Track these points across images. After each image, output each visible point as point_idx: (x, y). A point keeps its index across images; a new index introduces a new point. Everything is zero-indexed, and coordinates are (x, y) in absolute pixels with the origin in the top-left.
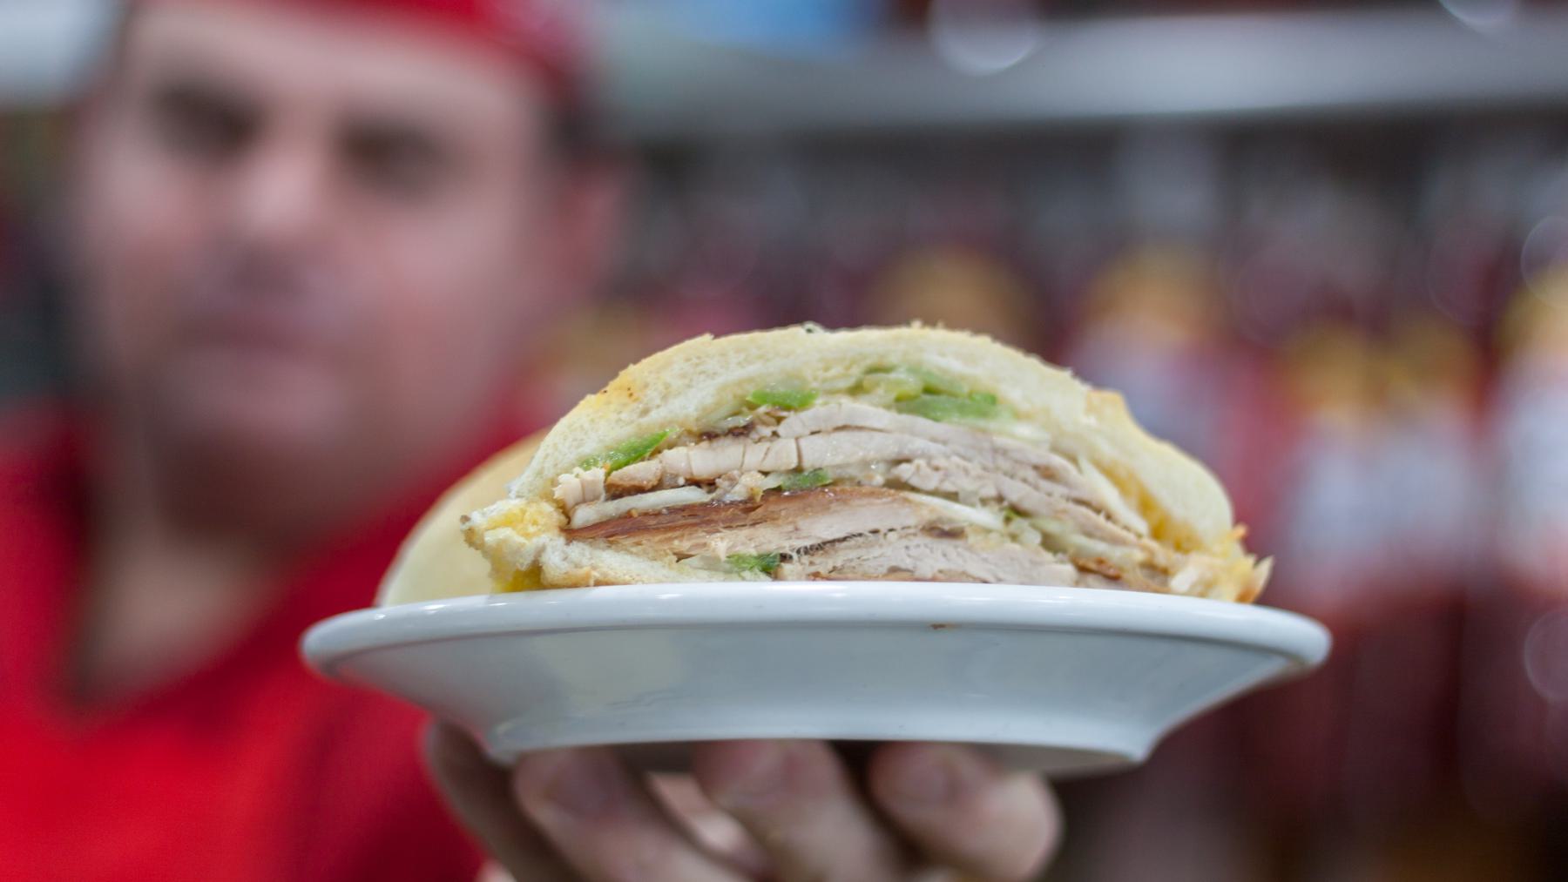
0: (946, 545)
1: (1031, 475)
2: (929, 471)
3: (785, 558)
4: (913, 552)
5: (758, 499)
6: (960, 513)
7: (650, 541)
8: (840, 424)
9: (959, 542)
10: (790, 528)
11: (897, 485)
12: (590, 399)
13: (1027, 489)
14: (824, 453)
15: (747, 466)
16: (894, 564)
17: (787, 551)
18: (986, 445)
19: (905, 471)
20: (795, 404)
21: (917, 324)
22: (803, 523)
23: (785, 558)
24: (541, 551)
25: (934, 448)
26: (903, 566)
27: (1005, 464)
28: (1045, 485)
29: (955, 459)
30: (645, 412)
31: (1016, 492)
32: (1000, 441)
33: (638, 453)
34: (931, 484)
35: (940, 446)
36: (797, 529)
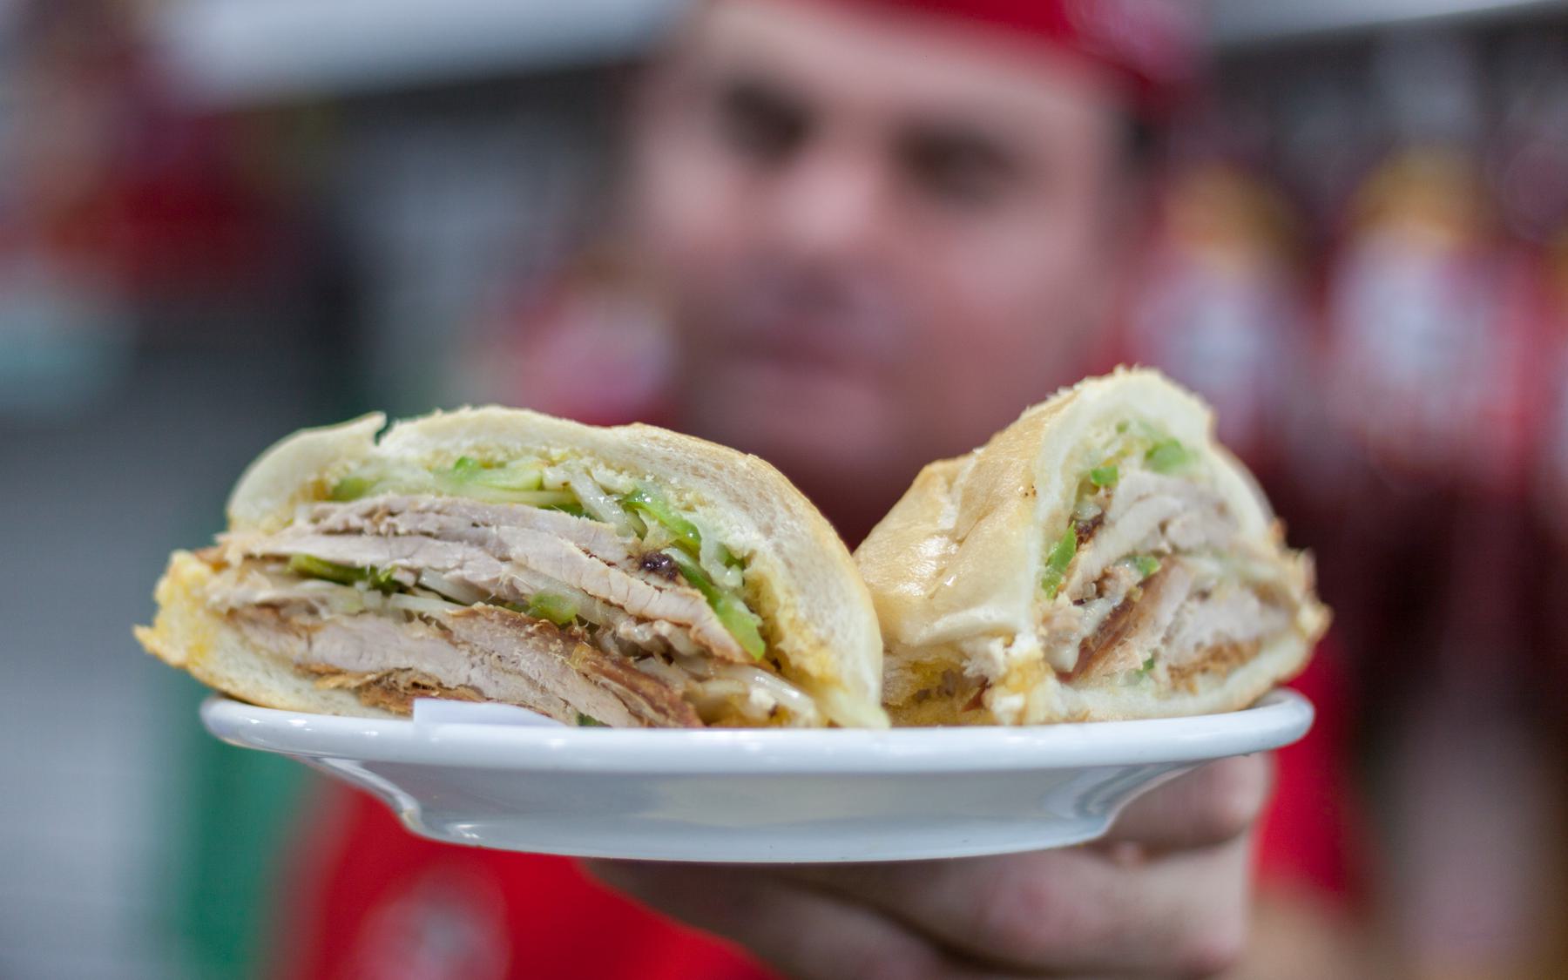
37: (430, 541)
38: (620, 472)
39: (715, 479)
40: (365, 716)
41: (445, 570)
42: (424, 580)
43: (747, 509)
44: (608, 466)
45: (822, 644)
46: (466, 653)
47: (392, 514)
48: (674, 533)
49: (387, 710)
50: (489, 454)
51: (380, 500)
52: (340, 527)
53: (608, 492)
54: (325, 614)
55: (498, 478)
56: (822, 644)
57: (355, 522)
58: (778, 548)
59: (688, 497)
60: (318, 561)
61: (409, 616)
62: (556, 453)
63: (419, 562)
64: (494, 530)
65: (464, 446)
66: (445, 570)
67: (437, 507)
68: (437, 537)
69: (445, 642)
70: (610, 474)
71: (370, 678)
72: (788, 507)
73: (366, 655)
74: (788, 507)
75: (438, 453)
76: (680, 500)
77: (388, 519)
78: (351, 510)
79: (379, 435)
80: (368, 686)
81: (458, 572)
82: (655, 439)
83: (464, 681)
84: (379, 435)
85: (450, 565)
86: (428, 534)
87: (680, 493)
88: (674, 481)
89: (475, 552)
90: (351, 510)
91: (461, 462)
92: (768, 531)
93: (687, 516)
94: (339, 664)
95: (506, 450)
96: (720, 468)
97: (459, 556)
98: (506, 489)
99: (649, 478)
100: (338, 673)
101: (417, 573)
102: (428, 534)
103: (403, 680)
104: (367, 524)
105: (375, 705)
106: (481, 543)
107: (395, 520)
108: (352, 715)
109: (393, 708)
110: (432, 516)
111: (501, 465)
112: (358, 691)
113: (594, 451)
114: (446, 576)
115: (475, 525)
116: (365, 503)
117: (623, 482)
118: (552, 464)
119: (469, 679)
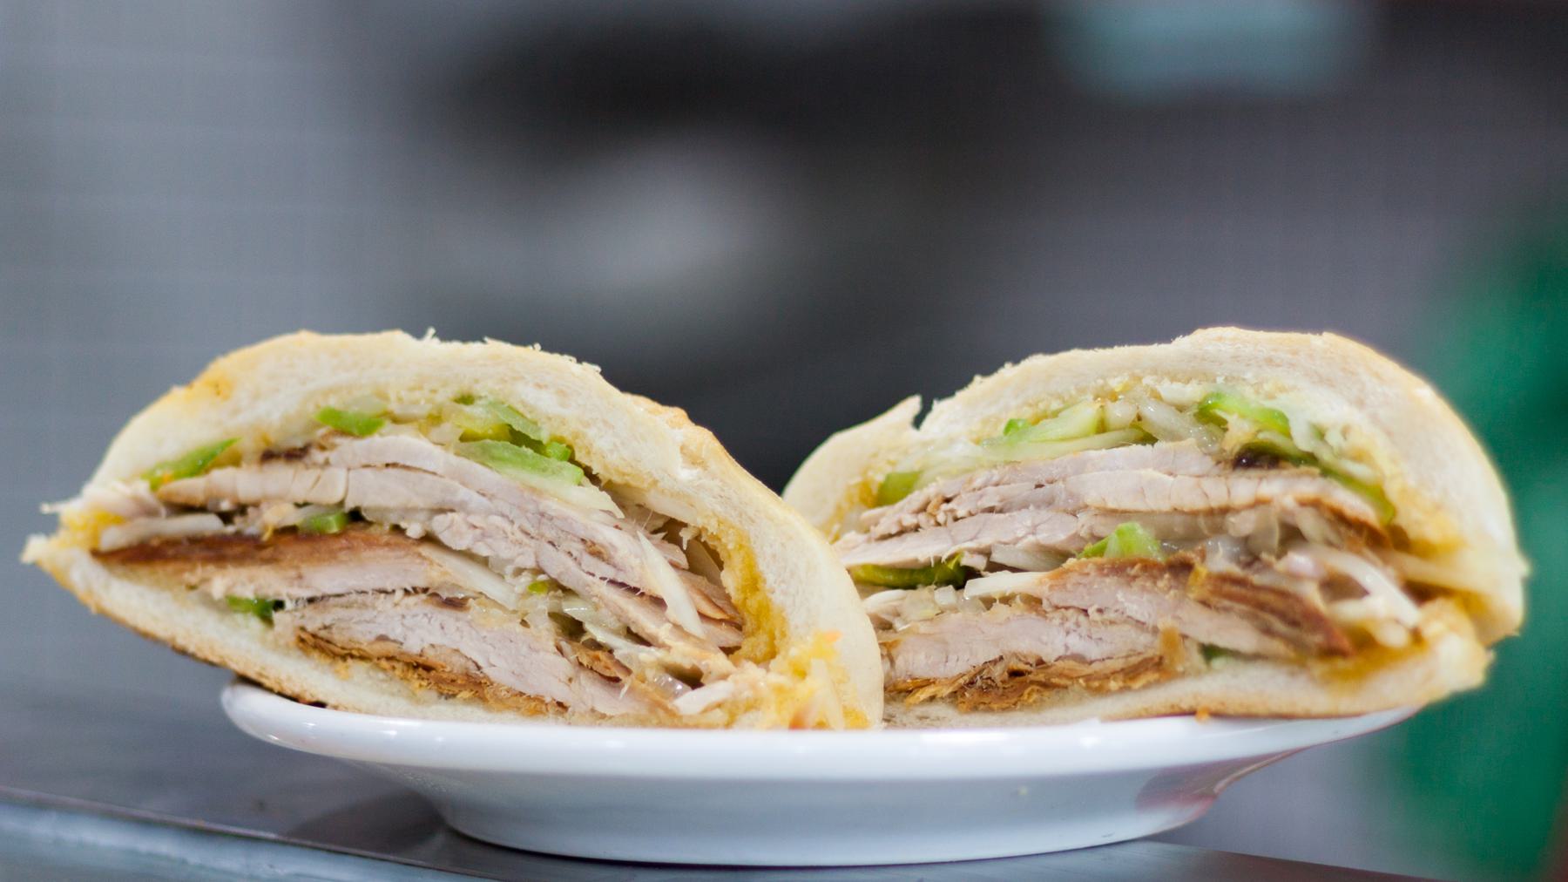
0: (447, 616)
1: (577, 548)
2: (464, 528)
3: (279, 605)
4: (408, 621)
5: (267, 536)
6: (473, 579)
7: (163, 571)
8: (390, 461)
9: (460, 614)
10: (293, 573)
11: (429, 539)
12: (178, 395)
13: (570, 562)
14: (371, 492)
15: (279, 495)
16: (382, 632)
17: (284, 597)
18: (531, 507)
19: (439, 525)
20: (356, 432)
21: (977, 378)
22: (306, 569)
23: (279, 605)
24: (1091, 528)
25: (476, 500)
26: (392, 637)
27: (550, 534)
28: (589, 562)
29: (497, 520)
30: (236, 412)
31: (558, 565)
32: (552, 506)
33: (204, 463)
34: (461, 544)
35: (484, 500)
36: (300, 577)
37: (995, 516)
38: (1188, 381)
39: (1292, 365)
40: (967, 727)
41: (1018, 540)
42: (997, 557)
43: (1332, 386)
44: (1173, 379)
45: (1438, 507)
46: (1057, 621)
47: (948, 501)
48: (1256, 422)
49: (990, 710)
50: (1042, 406)
51: (930, 491)
52: (894, 530)
53: (1181, 409)
54: (899, 626)
55: (1053, 429)
56: (1438, 507)
57: (909, 520)
58: (1375, 419)
59: (1267, 387)
60: (877, 568)
61: (988, 602)
62: (1116, 384)
63: (985, 541)
64: (1061, 485)
65: (1015, 409)
66: (1018, 540)
67: (996, 479)
68: (1001, 511)
69: (1033, 614)
70: (1177, 386)
71: (961, 681)
72: (1377, 375)
73: (953, 657)
74: (1377, 375)
75: (986, 421)
76: (1257, 392)
77: (945, 506)
78: (901, 509)
79: (918, 421)
80: (962, 688)
81: (1031, 538)
82: (1220, 339)
83: (1061, 652)
84: (918, 421)
85: (1020, 534)
86: (991, 510)
87: (1257, 387)
88: (1249, 376)
89: (1045, 514)
90: (901, 509)
91: (1011, 425)
92: (1360, 403)
93: (1268, 404)
94: (930, 674)
95: (1059, 397)
96: (1295, 353)
97: (1029, 523)
98: (1063, 440)
99: (1220, 380)
100: (928, 683)
101: (986, 553)
102: (991, 510)
103: (998, 672)
104: (922, 518)
105: (974, 708)
106: (1049, 503)
107: (951, 505)
108: (952, 727)
109: (995, 706)
110: (990, 489)
111: (1055, 414)
112: (956, 696)
113: (1158, 371)
114: (1020, 545)
115: (1039, 486)
116: (916, 498)
117: (1192, 392)
118: (1114, 397)
119: (1067, 648)
